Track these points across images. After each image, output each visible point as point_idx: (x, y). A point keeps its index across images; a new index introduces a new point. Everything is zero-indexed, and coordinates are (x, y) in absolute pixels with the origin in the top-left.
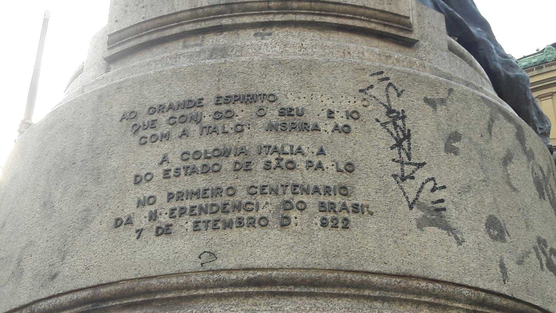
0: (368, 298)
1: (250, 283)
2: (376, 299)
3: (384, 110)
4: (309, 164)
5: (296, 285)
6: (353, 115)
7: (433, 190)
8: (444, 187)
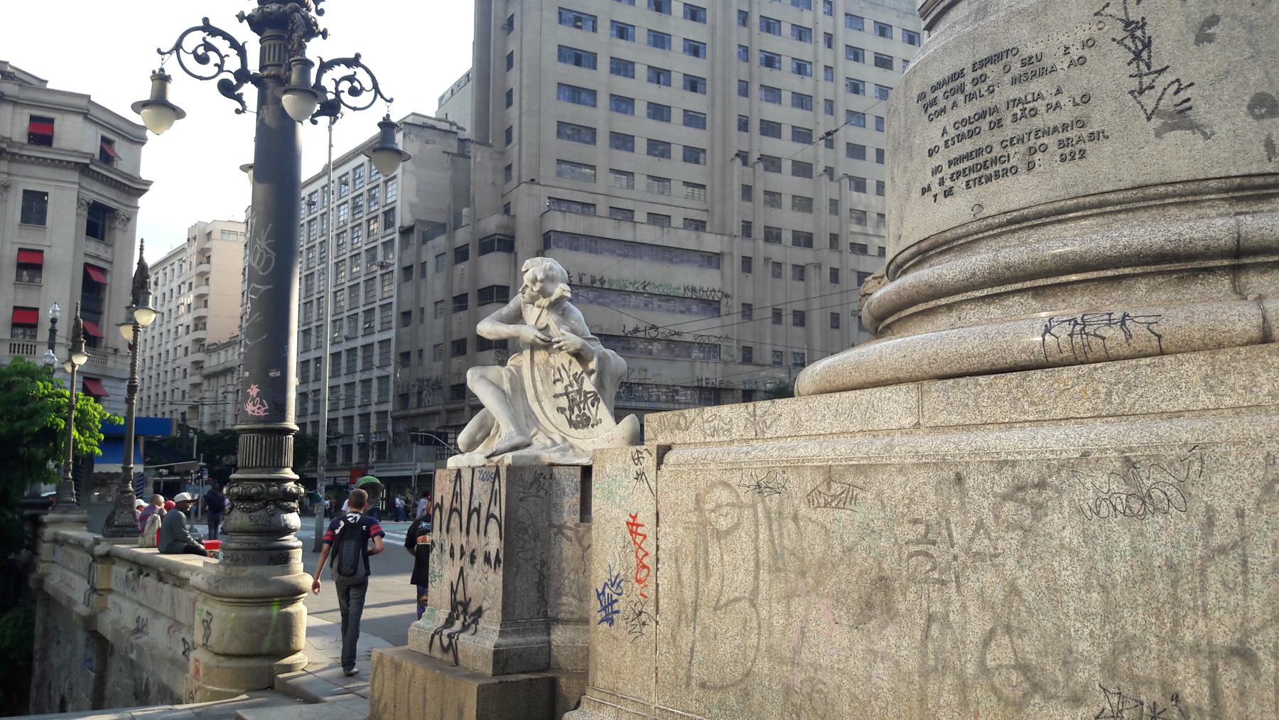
0: (1111, 213)
1: (1010, 222)
2: (1119, 212)
3: (1121, 25)
4: (1049, 107)
5: (1046, 216)
6: (1089, 43)
7: (1176, 93)
8: (1192, 84)
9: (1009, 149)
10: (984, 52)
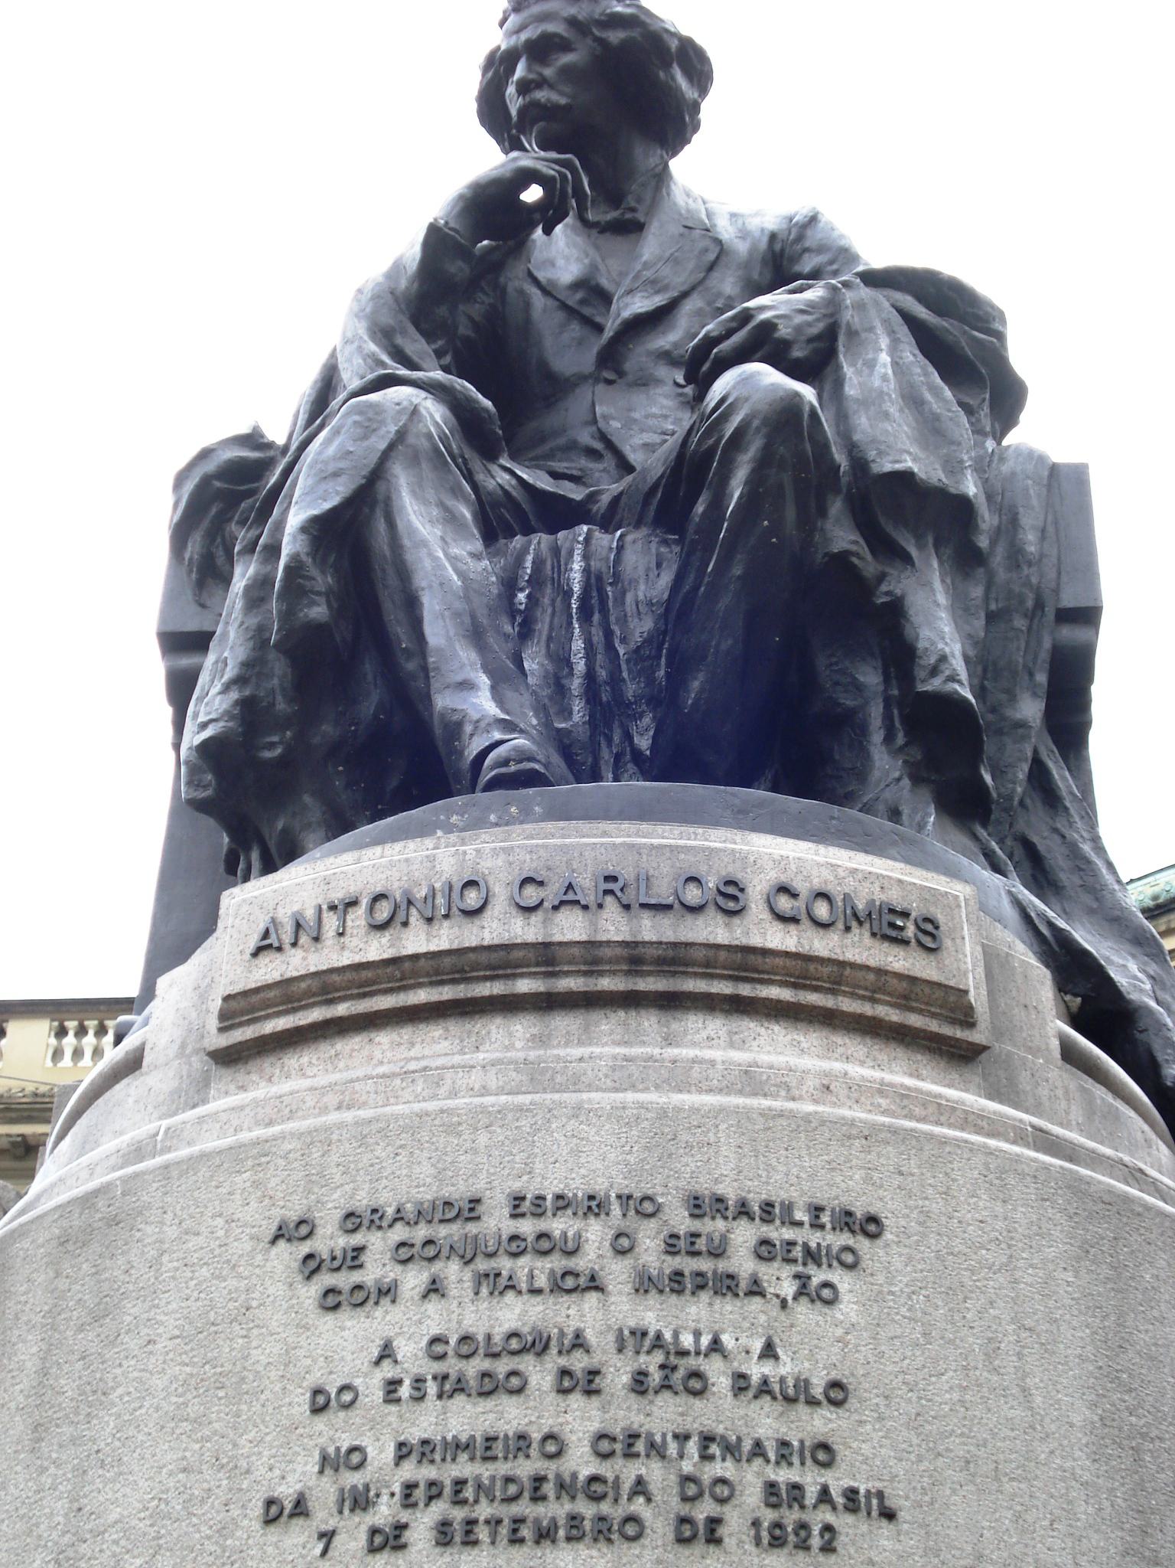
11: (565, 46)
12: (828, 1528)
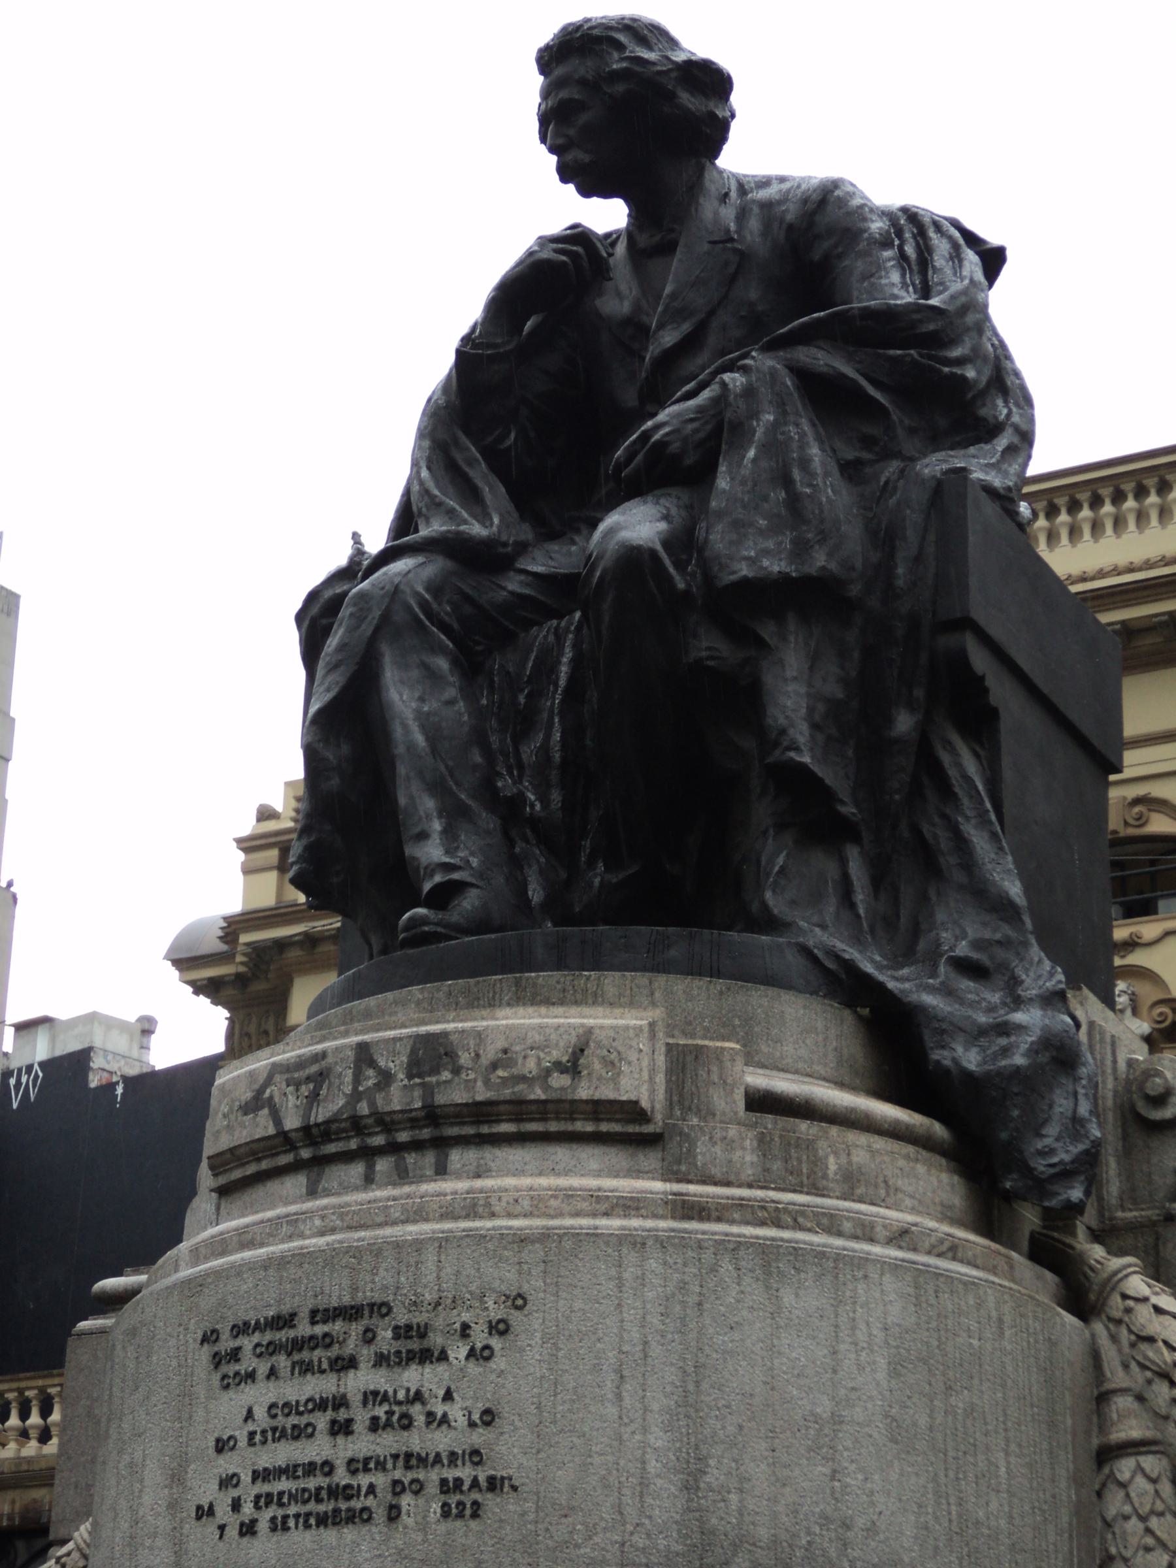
9: (360, 1476)
10: (338, 1293)
11: (581, 106)
12: (475, 1503)
